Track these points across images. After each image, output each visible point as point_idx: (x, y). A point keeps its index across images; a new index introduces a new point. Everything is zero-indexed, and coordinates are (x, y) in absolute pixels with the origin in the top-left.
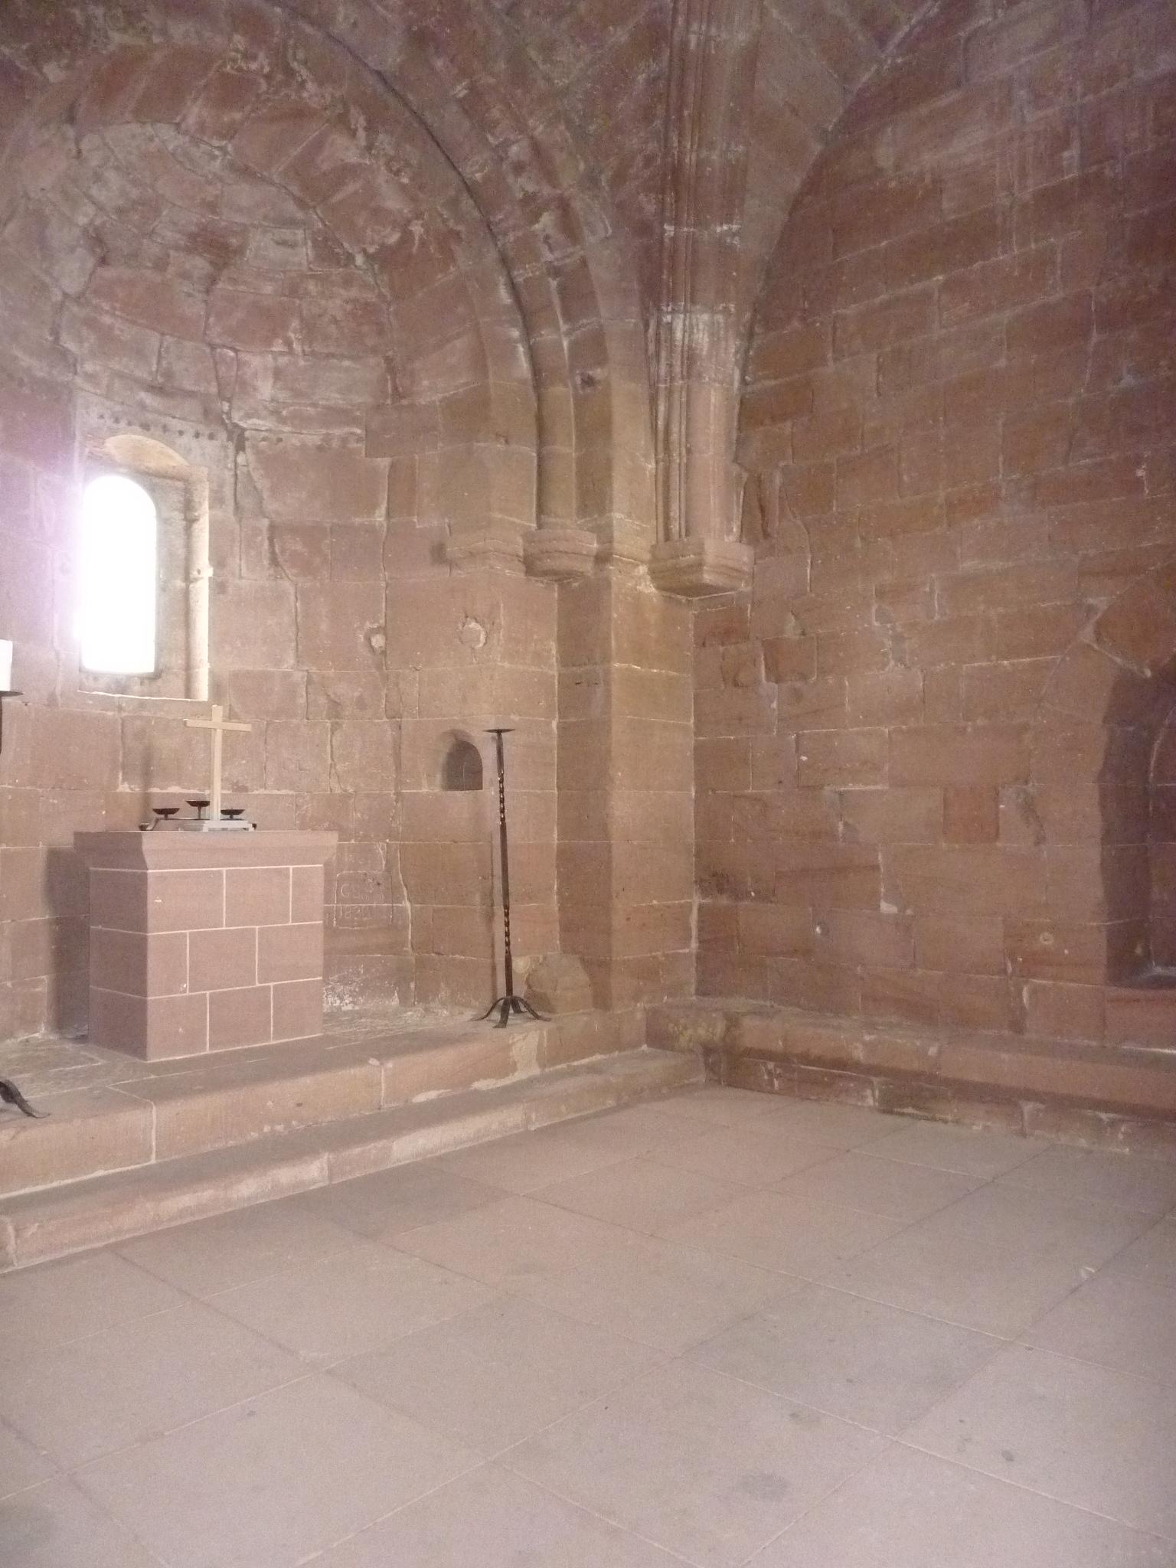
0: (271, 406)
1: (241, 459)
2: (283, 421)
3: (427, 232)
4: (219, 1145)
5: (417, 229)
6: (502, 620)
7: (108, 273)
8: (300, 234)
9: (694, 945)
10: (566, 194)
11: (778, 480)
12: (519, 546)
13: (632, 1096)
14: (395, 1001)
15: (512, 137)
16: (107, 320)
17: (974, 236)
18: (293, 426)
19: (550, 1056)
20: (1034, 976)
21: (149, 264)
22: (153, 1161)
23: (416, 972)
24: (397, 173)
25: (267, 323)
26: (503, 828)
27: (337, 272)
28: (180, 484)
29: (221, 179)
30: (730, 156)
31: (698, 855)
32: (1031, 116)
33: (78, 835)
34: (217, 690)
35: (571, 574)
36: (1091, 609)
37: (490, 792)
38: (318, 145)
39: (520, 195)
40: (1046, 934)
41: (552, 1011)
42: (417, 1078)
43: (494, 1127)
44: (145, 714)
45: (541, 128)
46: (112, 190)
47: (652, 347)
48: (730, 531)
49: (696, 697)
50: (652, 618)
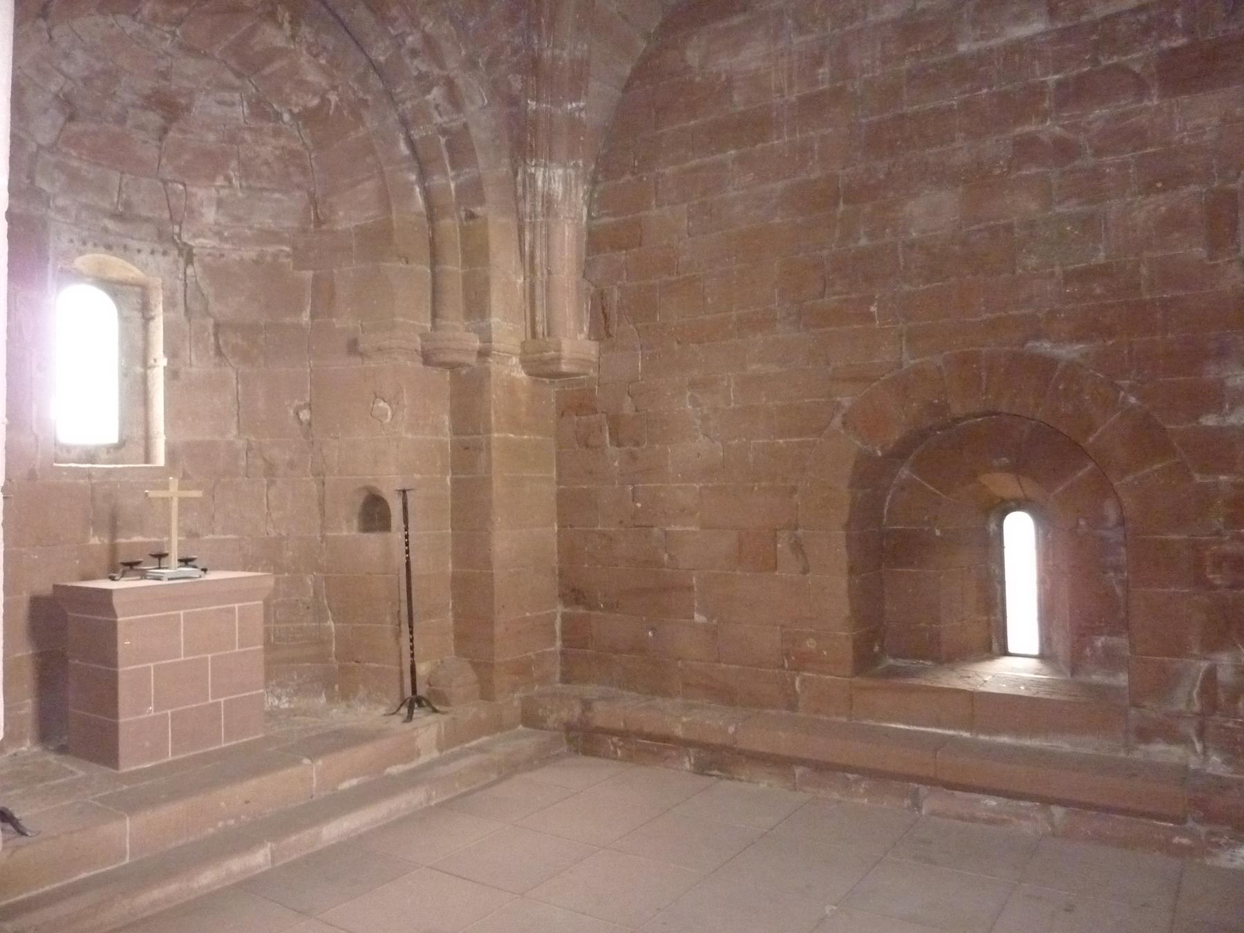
0: (216, 228)
1: (190, 271)
2: (226, 240)
3: (341, 100)
4: (181, 842)
5: (333, 98)
6: (406, 399)
7: (75, 128)
8: (237, 96)
9: (559, 643)
10: (452, 75)
11: (616, 295)
12: (418, 343)
13: (510, 768)
14: (323, 700)
15: (408, 30)
16: (75, 163)
17: (755, 126)
18: (233, 244)
19: (448, 740)
20: (804, 669)
21: (110, 119)
22: (127, 861)
23: (341, 675)
24: (316, 56)
25: (210, 163)
26: (408, 564)
27: (268, 126)
28: (137, 289)
29: (171, 55)
30: (578, 54)
31: (560, 575)
32: (797, 40)
33: (55, 587)
34: (171, 454)
35: (461, 365)
36: (839, 406)
37: (397, 535)
38: (252, 31)
39: (415, 73)
40: (812, 640)
41: (447, 704)
42: (341, 771)
43: (403, 806)
44: (112, 479)
45: (431, 24)
46: (78, 64)
47: (520, 190)
48: (581, 331)
49: (558, 454)
50: (523, 396)
